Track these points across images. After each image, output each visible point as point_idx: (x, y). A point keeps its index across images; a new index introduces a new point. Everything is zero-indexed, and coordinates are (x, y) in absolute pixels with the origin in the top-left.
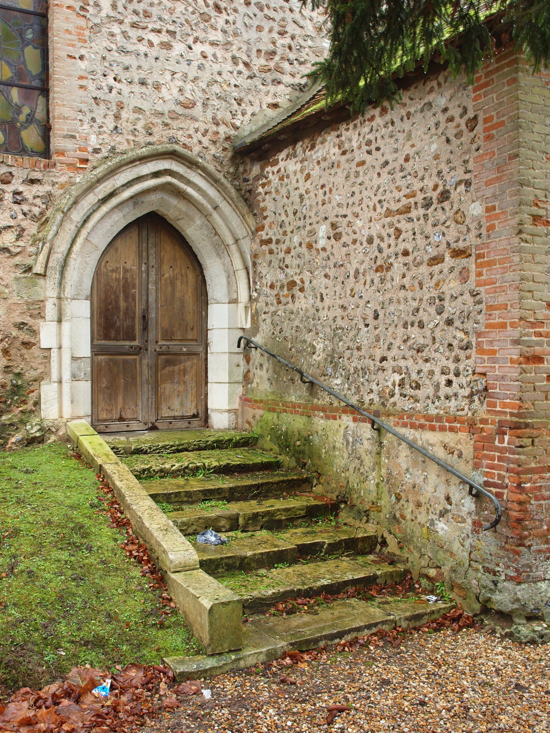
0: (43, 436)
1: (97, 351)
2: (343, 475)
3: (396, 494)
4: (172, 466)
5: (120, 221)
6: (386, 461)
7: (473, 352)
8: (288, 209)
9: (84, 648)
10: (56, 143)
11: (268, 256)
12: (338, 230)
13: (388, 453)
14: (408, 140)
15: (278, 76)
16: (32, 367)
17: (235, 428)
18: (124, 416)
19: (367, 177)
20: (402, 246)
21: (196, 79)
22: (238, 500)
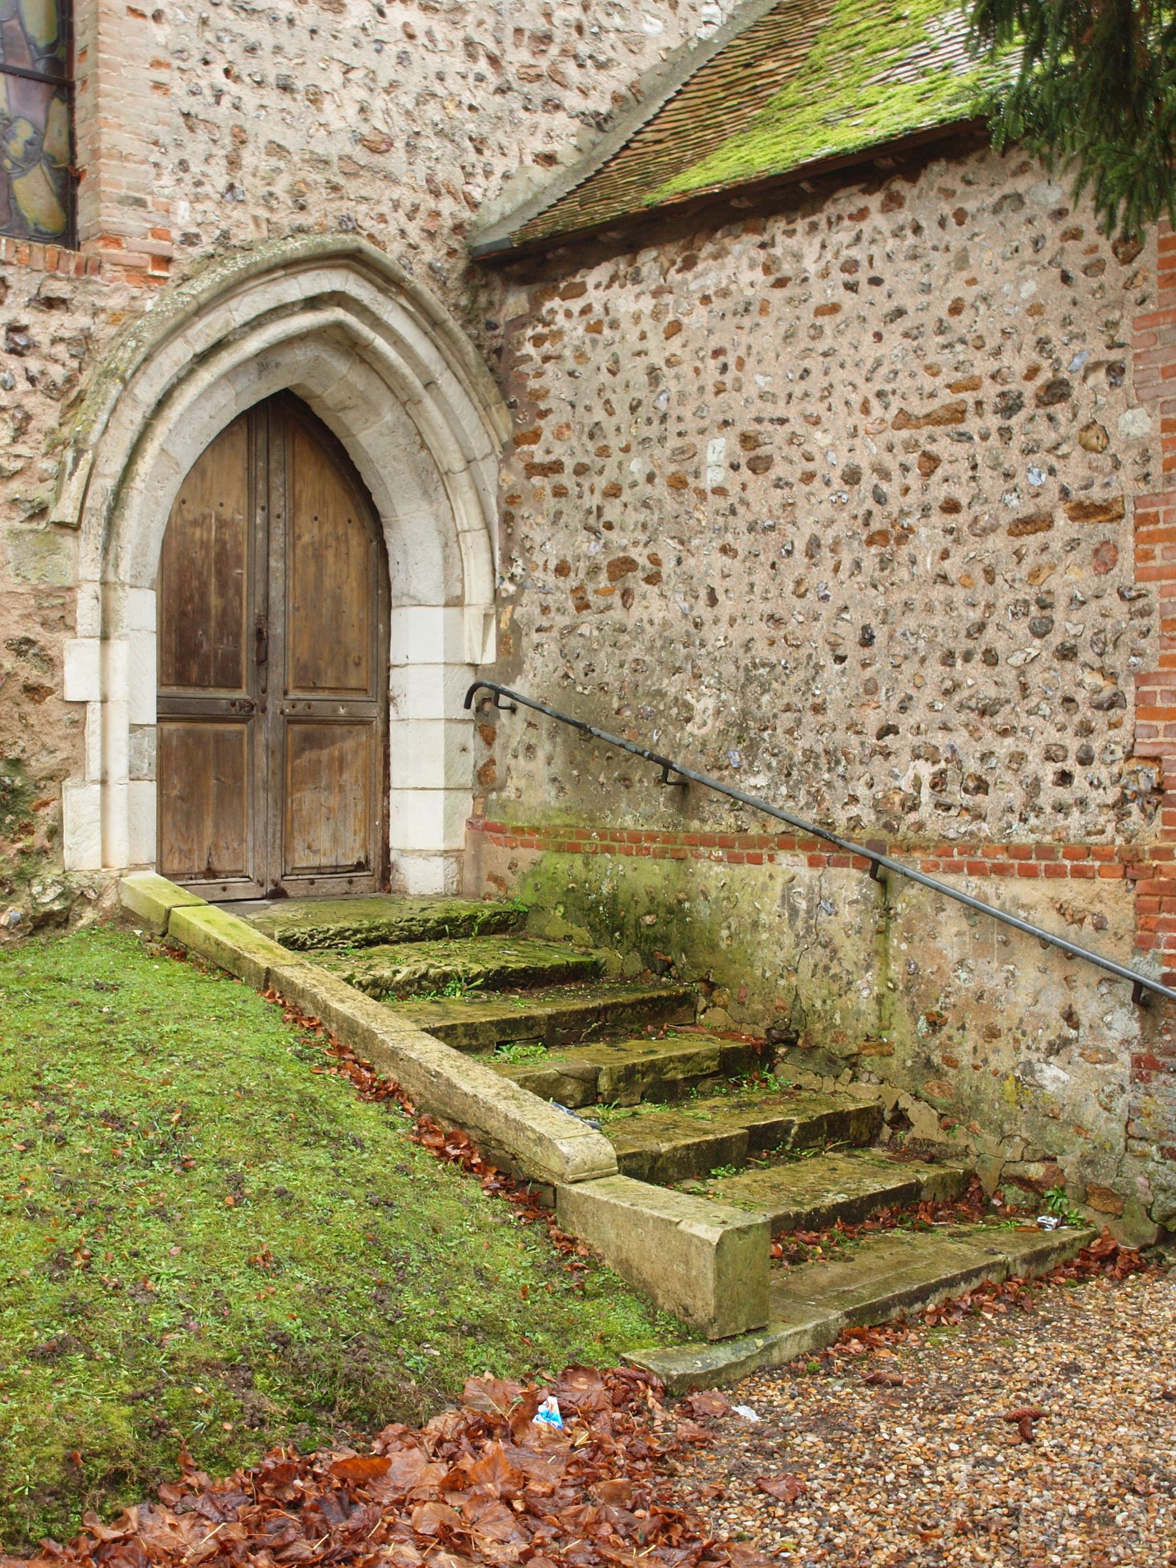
0: (68, 909)
1: (168, 710)
2: (782, 982)
3: (929, 1016)
4: (396, 972)
5: (229, 404)
6: (904, 946)
7: (1128, 714)
8: (613, 398)
9: (471, 1340)
10: (97, 211)
11: (551, 503)
12: (760, 451)
13: (909, 927)
14: (960, 269)
15: (555, 91)
16: (44, 746)
17: (458, 894)
18: (217, 866)
19: (844, 341)
20: (939, 492)
21: (393, 85)
22: (564, 1043)
